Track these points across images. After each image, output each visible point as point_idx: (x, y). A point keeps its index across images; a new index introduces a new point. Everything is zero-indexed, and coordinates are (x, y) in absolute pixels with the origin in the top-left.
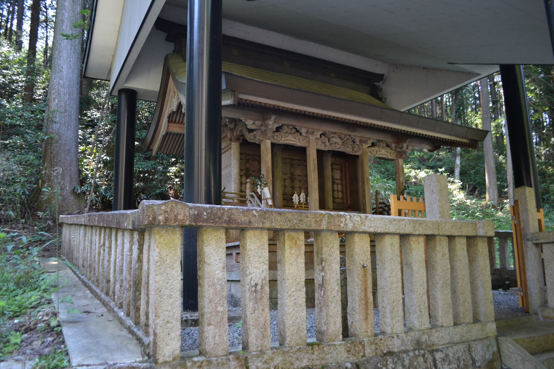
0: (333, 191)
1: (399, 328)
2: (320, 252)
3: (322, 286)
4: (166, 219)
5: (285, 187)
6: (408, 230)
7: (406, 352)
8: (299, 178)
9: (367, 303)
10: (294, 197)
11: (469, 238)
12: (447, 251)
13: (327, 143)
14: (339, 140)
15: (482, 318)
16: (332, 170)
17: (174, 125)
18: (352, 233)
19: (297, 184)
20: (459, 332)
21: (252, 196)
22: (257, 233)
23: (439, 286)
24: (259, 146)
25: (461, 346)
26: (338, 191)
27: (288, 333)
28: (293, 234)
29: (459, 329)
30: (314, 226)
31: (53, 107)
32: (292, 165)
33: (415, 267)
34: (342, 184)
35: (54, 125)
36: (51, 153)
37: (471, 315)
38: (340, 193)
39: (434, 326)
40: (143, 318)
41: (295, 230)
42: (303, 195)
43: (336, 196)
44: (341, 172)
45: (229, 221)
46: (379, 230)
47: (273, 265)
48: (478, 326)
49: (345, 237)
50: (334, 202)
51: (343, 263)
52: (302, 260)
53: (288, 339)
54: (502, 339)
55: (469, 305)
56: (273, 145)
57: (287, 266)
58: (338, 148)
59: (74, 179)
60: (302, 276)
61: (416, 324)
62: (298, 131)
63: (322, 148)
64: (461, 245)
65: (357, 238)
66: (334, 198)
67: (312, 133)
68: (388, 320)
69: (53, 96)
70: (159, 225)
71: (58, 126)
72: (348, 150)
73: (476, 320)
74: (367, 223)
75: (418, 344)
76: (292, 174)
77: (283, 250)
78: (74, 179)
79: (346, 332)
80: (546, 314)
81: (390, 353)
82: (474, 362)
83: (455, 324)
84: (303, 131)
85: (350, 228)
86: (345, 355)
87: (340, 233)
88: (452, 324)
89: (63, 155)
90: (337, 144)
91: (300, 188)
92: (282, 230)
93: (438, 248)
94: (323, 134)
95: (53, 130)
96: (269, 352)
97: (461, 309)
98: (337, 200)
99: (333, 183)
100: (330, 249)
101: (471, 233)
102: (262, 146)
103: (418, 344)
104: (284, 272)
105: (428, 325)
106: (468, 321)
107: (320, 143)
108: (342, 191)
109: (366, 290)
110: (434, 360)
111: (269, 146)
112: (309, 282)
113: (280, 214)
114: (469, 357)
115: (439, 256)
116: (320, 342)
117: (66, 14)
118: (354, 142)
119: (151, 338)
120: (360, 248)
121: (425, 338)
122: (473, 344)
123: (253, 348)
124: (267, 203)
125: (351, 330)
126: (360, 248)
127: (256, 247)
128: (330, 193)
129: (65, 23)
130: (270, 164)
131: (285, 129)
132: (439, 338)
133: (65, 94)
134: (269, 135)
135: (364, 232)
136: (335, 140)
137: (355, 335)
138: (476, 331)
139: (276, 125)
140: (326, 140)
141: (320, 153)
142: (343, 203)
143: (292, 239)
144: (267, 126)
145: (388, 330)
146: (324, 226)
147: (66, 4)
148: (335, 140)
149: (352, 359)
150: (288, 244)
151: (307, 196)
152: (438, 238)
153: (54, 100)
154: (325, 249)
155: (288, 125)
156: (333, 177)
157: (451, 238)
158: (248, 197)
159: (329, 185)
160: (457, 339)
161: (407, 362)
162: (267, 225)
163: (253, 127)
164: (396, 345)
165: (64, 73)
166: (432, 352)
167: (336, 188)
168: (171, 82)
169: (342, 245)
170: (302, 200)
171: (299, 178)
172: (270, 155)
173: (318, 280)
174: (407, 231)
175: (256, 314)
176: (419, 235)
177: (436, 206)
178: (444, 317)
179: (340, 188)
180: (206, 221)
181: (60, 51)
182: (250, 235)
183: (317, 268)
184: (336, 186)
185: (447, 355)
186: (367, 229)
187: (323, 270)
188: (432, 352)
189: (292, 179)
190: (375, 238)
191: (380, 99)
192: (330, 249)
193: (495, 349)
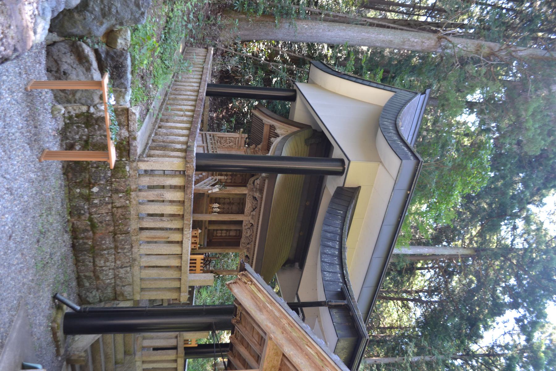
0: (222, 230)
1: (142, 252)
2: (175, 220)
3: (162, 220)
4: (188, 167)
5: (224, 199)
6: (184, 258)
7: (132, 254)
8: (230, 208)
9: (154, 238)
10: (217, 204)
11: (180, 288)
12: (174, 277)
13: (247, 227)
14: (248, 235)
15: (142, 293)
16: (236, 230)
17: (268, 128)
18: (183, 233)
19: (226, 206)
20: (138, 281)
21: (216, 180)
22: (183, 196)
23: (159, 272)
24: (245, 186)
25: (131, 280)
26: (221, 233)
27: (144, 206)
28: (182, 210)
29: (139, 280)
30: (185, 218)
31: (302, 24)
32: (239, 204)
33: (167, 261)
34: (226, 236)
35: (288, 24)
36: (267, 21)
37: (144, 287)
38: (220, 234)
39: (141, 268)
40: (152, 152)
41: (184, 210)
42: (218, 210)
43: (218, 232)
44: (235, 236)
45: (187, 187)
46: (184, 245)
47: (172, 202)
48: (139, 290)
49: (181, 230)
50: (214, 230)
51: (171, 229)
52: (172, 213)
53: (141, 206)
54: (132, 302)
55: (149, 286)
56: (245, 194)
57: (170, 207)
58: (244, 234)
59: (246, 37)
60: (165, 212)
61: (143, 260)
62: (254, 209)
63: (244, 224)
64: (176, 284)
65: (180, 235)
66: (217, 230)
67: (252, 218)
68: (145, 247)
69: (310, 24)
70: (186, 164)
71: (287, 27)
72: (243, 240)
73: (142, 289)
74: (187, 240)
75: (134, 260)
76: (233, 204)
77: (176, 206)
78: (246, 37)
79: (142, 229)
80: (139, 338)
81: (132, 247)
82: (124, 286)
83: (141, 279)
84: (254, 213)
85: (185, 233)
86: (133, 228)
87: (183, 228)
88: (142, 277)
89: (265, 30)
90: (246, 233)
91: (224, 208)
92: (184, 206)
93: (176, 272)
94: (252, 225)
95: (284, 23)
96: (137, 199)
97: (148, 282)
98: (215, 232)
99: (227, 230)
100: (176, 224)
101: (182, 289)
102: (244, 188)
103: (134, 260)
104: (168, 205)
105: (142, 265)
106: (142, 285)
107: (247, 223)
108: (221, 236)
109: (159, 238)
110: (126, 267)
111: (244, 192)
112: (162, 215)
113: (190, 205)
114: (126, 284)
115: (172, 273)
116: (139, 218)
117: (374, 36)
118: (248, 244)
119: (146, 159)
120: (176, 237)
121: (137, 263)
122: (131, 287)
123: (140, 193)
124: (209, 190)
125: (143, 231)
126: (176, 237)
127: (178, 196)
128: (219, 228)
129: (366, 35)
130: (233, 192)
131: (255, 202)
132: (136, 269)
133: (311, 33)
134: (251, 193)
135: (183, 239)
136: (249, 232)
137: (140, 233)
138: (137, 289)
139: (257, 197)
140: (249, 227)
141: (241, 222)
142: (213, 236)
143: (181, 209)
144: (256, 191)
145: (141, 247)
146: (185, 222)
147: (381, 36)
148: (249, 232)
149: (132, 231)
150: (179, 207)
151: (218, 213)
152: (180, 272)
153: (307, 25)
154: (176, 222)
155: (257, 204)
156: (231, 230)
157: (180, 279)
158: (215, 178)
159: (224, 227)
160: (135, 278)
161: (128, 254)
162: (186, 200)
163: (255, 184)
164: (135, 250)
165: (328, 33)
166: (130, 266)
167: (223, 232)
168: (295, 129)
169: (178, 229)
170: (215, 209)
171: (230, 208)
172: (238, 193)
173: (164, 218)
174: (183, 258)
175: (152, 195)
176: (181, 263)
177: (198, 278)
178: (147, 273)
179: (224, 235)
180: (187, 179)
181: (344, 30)
182: (182, 194)
183: (169, 218)
184: (225, 232)
185: (128, 273)
186: (184, 239)
187: (168, 221)
188: (130, 266)
189: (230, 203)
190: (180, 243)
191: (284, 265)
192: (176, 224)
193: (128, 298)
